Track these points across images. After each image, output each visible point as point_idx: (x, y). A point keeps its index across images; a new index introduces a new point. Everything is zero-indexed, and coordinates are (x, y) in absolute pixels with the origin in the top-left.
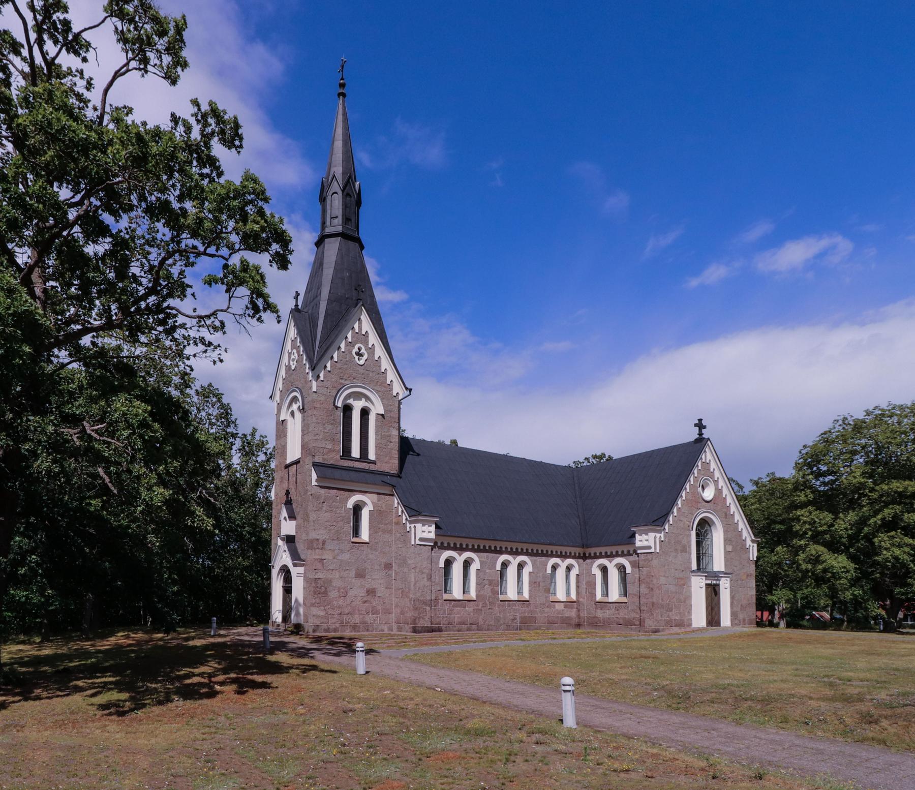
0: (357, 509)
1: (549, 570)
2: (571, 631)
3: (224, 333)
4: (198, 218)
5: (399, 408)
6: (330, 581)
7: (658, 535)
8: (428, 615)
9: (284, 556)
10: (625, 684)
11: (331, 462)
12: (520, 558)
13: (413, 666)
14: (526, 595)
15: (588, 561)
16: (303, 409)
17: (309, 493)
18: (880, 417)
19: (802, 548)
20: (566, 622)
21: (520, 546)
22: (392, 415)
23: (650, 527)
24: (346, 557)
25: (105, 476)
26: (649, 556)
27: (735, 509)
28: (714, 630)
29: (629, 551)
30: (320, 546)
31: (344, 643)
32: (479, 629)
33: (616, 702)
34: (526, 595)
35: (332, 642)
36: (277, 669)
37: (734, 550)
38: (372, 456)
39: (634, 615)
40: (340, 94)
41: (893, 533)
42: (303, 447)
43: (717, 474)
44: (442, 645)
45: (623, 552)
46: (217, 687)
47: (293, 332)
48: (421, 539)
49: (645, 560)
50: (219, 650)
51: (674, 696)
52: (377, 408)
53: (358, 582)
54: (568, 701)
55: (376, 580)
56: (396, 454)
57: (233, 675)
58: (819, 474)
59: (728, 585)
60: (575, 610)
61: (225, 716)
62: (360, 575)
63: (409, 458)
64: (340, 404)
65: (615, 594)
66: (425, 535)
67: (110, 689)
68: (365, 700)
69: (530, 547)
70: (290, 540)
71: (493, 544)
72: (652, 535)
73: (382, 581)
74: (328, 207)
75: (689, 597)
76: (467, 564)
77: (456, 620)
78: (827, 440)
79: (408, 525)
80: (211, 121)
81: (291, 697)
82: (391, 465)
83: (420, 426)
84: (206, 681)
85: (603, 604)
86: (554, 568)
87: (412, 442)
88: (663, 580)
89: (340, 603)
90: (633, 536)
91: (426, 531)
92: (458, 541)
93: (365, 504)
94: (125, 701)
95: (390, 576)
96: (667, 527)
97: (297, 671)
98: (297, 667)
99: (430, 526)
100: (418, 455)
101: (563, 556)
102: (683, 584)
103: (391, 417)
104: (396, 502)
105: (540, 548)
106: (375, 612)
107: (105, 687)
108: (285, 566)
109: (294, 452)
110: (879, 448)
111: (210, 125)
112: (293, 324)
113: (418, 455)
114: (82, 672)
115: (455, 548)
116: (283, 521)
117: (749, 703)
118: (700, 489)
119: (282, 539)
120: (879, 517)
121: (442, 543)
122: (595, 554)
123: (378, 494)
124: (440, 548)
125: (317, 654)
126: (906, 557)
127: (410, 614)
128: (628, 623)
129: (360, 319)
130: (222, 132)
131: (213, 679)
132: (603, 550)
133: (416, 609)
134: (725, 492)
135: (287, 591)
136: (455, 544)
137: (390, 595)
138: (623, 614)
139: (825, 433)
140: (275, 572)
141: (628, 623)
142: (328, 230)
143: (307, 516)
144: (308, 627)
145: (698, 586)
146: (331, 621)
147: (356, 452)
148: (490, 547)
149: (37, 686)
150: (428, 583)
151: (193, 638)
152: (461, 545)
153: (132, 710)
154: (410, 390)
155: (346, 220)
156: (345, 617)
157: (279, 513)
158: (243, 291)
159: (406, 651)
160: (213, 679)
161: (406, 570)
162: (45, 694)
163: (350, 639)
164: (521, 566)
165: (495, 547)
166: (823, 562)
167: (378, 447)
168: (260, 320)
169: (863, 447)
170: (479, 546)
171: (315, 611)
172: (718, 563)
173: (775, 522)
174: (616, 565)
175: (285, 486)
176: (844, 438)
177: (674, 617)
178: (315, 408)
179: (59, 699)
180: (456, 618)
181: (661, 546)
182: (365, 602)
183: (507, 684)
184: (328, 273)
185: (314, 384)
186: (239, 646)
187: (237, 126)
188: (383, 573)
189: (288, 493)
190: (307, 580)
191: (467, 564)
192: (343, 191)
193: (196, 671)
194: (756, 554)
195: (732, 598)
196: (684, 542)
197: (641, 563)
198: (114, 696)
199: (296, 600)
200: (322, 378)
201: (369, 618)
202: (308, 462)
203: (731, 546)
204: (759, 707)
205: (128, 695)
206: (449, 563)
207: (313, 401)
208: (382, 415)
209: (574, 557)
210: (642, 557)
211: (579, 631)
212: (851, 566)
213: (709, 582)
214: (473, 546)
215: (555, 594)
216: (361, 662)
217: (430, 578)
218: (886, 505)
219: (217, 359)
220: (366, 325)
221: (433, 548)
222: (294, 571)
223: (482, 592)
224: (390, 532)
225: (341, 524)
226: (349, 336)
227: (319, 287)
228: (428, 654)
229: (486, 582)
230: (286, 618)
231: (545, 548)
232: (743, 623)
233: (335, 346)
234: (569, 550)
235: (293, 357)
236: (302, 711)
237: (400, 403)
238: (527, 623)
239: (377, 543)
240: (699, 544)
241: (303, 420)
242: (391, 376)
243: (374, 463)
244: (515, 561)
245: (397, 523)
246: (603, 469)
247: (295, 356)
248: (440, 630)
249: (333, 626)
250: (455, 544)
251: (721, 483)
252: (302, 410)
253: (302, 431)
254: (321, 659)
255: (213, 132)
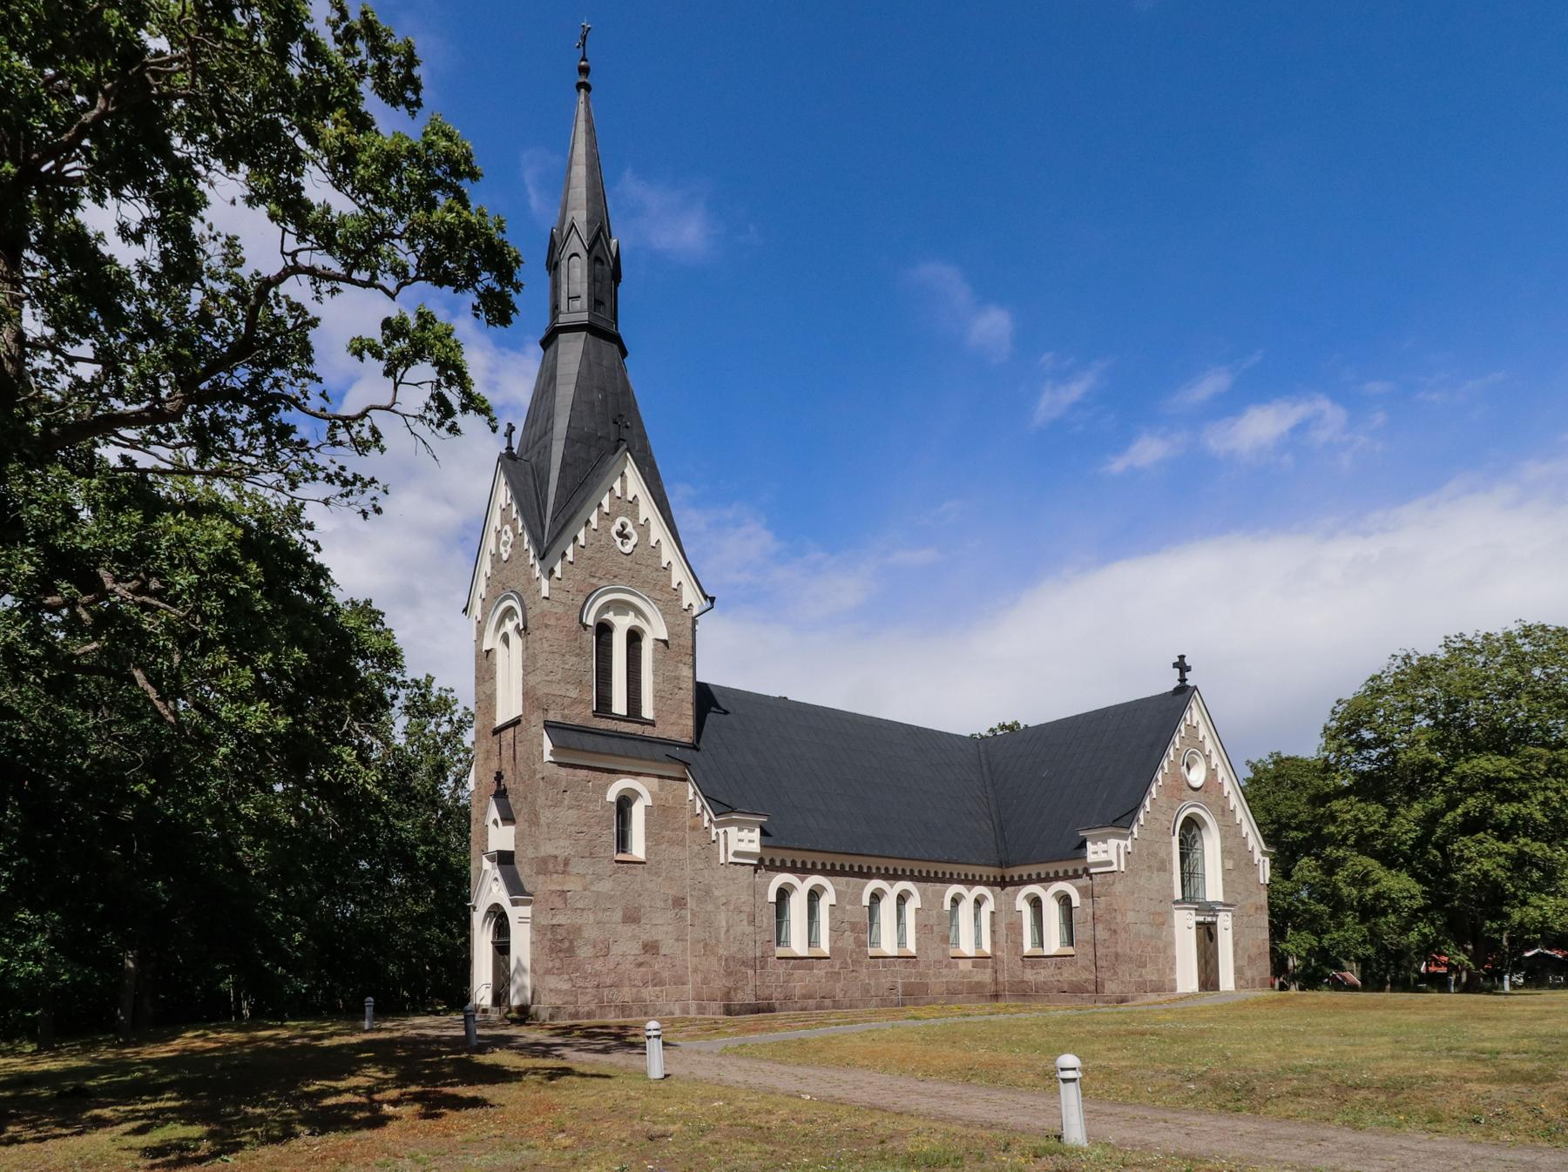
0: (624, 804)
1: (947, 905)
2: (989, 1006)
3: (382, 450)
4: (345, 145)
5: (694, 631)
6: (577, 930)
7: (1122, 843)
8: (751, 985)
9: (495, 889)
10: (1131, 1073)
11: (577, 721)
12: (902, 885)
13: (745, 1064)
14: (911, 948)
15: (1009, 889)
16: (525, 628)
17: (539, 776)
18: (1461, 650)
19: (1339, 863)
20: (976, 990)
21: (901, 865)
22: (682, 641)
23: (1110, 830)
24: (605, 886)
25: (148, 687)
26: (1110, 878)
27: (1236, 802)
28: (1210, 998)
29: (1076, 871)
30: (560, 868)
31: (609, 1034)
32: (837, 1005)
33: (1125, 1104)
34: (911, 948)
35: (589, 1034)
36: (498, 1075)
37: (1237, 867)
38: (647, 712)
39: (1085, 975)
40: (580, 86)
41: (1481, 835)
42: (527, 695)
43: (1209, 745)
44: (781, 1030)
45: (1066, 872)
46: (388, 1109)
47: (504, 495)
48: (736, 854)
49: (1103, 884)
50: (383, 1052)
51: (1225, 1090)
52: (656, 629)
53: (628, 929)
54: (1071, 1097)
55: (660, 926)
56: (689, 710)
57: (414, 1089)
58: (1362, 745)
59: (1229, 924)
60: (989, 970)
61: (411, 1157)
62: (631, 918)
63: (711, 718)
64: (590, 620)
65: (1054, 943)
66: (744, 847)
67: (167, 1121)
68: (685, 1118)
69: (916, 866)
70: (505, 859)
71: (856, 862)
72: (1113, 842)
73: (670, 928)
74: (563, 279)
75: (1172, 944)
76: (814, 896)
77: (797, 992)
78: (1376, 689)
79: (714, 831)
80: (361, 45)
81: (537, 1120)
82: (681, 727)
83: (735, 659)
84: (364, 1100)
85: (1035, 960)
86: (956, 901)
87: (715, 692)
88: (1131, 917)
89: (598, 967)
90: (1082, 845)
91: (744, 840)
92: (799, 857)
93: (637, 794)
94: (201, 1139)
95: (682, 918)
96: (1135, 830)
97: (538, 1078)
98: (535, 1071)
99: (751, 831)
100: (726, 712)
101: (970, 882)
102: (1162, 922)
103: (681, 647)
104: (691, 791)
105: (933, 868)
106: (658, 982)
107: (158, 1118)
108: (497, 905)
109: (509, 706)
110: (1452, 706)
111: (358, 54)
112: (503, 480)
113: (726, 712)
114: (103, 1094)
115: (793, 869)
116: (491, 827)
117: (1363, 1093)
118: (1184, 768)
119: (491, 859)
120: (1459, 811)
121: (772, 861)
122: (1021, 877)
123: (660, 777)
124: (768, 869)
125: (565, 1051)
126: (1500, 872)
127: (719, 984)
128: (1077, 989)
129: (623, 474)
130: (383, 68)
131: (377, 1097)
132: (1033, 870)
133: (729, 974)
134: (1221, 774)
135: (502, 949)
136: (793, 862)
137: (684, 951)
138: (1068, 975)
139: (1372, 680)
140: (477, 918)
141: (1077, 989)
142: (563, 319)
143: (536, 815)
144: (543, 1009)
145: (1184, 924)
146: (582, 999)
147: (619, 705)
148: (851, 867)
149: (10, 1119)
150: (751, 929)
151: (332, 1035)
152: (804, 863)
153: (215, 1155)
154: (712, 600)
155: (596, 303)
156: (606, 991)
157: (485, 813)
158: (424, 371)
159: (720, 1042)
160: (377, 1097)
161: (710, 907)
162: (31, 1134)
163: (621, 1027)
164: (902, 899)
165: (860, 867)
166: (1375, 883)
167: (658, 696)
168: (453, 429)
169: (1429, 701)
170: (833, 865)
171: (553, 982)
172: (1214, 890)
173: (1287, 827)
174: (1056, 895)
175: (494, 765)
176: (1401, 686)
177: (1149, 977)
178: (547, 626)
179: (58, 1142)
180: (798, 988)
181: (1127, 861)
182: (640, 965)
183: (922, 1085)
184: (565, 392)
185: (545, 584)
186: (420, 1046)
187: (411, 61)
188: (671, 914)
189: (499, 777)
190: (537, 929)
191: (814, 896)
192: (589, 252)
193: (341, 1084)
194: (1268, 875)
195: (1235, 944)
196: (1162, 854)
197: (1096, 889)
198: (176, 1131)
199: (519, 961)
200: (558, 574)
201: (648, 993)
202: (537, 720)
203: (1232, 861)
204: (1382, 1098)
205: (206, 1128)
206: (783, 894)
207: (543, 614)
208: (665, 642)
209: (987, 884)
210: (1097, 879)
211: (1001, 1004)
212: (1416, 888)
213: (1201, 919)
214: (824, 865)
215: (957, 944)
216: (655, 1061)
217: (752, 922)
218: (1471, 791)
219: (369, 508)
220: (634, 484)
221: (756, 868)
222: (514, 914)
223: (840, 944)
224: (681, 843)
225: (596, 830)
226: (606, 501)
227: (550, 417)
228: (764, 1045)
229: (845, 925)
230: (500, 997)
231: (940, 868)
232: (1251, 984)
233: (580, 518)
234: (978, 871)
235: (504, 538)
236: (568, 1142)
237: (694, 622)
238: (913, 995)
239: (659, 862)
240: (1184, 857)
241: (526, 648)
242: (679, 574)
243: (652, 723)
244: (892, 890)
245: (694, 828)
246: (1012, 748)
247: (509, 536)
248: (770, 1009)
249: (586, 1007)
250: (793, 862)
251: (1215, 760)
252: (523, 631)
253: (524, 667)
254: (574, 1058)
255: (362, 68)
